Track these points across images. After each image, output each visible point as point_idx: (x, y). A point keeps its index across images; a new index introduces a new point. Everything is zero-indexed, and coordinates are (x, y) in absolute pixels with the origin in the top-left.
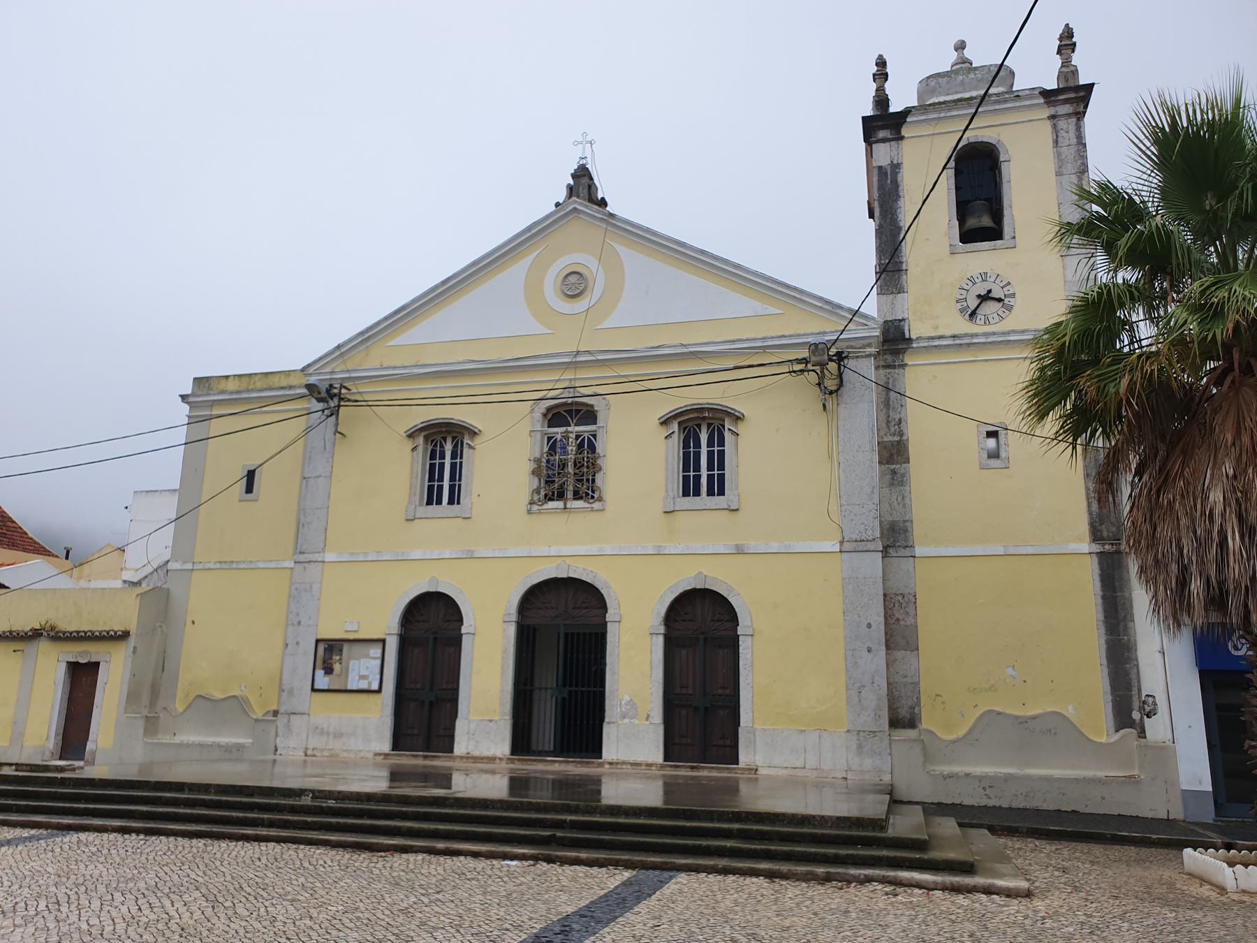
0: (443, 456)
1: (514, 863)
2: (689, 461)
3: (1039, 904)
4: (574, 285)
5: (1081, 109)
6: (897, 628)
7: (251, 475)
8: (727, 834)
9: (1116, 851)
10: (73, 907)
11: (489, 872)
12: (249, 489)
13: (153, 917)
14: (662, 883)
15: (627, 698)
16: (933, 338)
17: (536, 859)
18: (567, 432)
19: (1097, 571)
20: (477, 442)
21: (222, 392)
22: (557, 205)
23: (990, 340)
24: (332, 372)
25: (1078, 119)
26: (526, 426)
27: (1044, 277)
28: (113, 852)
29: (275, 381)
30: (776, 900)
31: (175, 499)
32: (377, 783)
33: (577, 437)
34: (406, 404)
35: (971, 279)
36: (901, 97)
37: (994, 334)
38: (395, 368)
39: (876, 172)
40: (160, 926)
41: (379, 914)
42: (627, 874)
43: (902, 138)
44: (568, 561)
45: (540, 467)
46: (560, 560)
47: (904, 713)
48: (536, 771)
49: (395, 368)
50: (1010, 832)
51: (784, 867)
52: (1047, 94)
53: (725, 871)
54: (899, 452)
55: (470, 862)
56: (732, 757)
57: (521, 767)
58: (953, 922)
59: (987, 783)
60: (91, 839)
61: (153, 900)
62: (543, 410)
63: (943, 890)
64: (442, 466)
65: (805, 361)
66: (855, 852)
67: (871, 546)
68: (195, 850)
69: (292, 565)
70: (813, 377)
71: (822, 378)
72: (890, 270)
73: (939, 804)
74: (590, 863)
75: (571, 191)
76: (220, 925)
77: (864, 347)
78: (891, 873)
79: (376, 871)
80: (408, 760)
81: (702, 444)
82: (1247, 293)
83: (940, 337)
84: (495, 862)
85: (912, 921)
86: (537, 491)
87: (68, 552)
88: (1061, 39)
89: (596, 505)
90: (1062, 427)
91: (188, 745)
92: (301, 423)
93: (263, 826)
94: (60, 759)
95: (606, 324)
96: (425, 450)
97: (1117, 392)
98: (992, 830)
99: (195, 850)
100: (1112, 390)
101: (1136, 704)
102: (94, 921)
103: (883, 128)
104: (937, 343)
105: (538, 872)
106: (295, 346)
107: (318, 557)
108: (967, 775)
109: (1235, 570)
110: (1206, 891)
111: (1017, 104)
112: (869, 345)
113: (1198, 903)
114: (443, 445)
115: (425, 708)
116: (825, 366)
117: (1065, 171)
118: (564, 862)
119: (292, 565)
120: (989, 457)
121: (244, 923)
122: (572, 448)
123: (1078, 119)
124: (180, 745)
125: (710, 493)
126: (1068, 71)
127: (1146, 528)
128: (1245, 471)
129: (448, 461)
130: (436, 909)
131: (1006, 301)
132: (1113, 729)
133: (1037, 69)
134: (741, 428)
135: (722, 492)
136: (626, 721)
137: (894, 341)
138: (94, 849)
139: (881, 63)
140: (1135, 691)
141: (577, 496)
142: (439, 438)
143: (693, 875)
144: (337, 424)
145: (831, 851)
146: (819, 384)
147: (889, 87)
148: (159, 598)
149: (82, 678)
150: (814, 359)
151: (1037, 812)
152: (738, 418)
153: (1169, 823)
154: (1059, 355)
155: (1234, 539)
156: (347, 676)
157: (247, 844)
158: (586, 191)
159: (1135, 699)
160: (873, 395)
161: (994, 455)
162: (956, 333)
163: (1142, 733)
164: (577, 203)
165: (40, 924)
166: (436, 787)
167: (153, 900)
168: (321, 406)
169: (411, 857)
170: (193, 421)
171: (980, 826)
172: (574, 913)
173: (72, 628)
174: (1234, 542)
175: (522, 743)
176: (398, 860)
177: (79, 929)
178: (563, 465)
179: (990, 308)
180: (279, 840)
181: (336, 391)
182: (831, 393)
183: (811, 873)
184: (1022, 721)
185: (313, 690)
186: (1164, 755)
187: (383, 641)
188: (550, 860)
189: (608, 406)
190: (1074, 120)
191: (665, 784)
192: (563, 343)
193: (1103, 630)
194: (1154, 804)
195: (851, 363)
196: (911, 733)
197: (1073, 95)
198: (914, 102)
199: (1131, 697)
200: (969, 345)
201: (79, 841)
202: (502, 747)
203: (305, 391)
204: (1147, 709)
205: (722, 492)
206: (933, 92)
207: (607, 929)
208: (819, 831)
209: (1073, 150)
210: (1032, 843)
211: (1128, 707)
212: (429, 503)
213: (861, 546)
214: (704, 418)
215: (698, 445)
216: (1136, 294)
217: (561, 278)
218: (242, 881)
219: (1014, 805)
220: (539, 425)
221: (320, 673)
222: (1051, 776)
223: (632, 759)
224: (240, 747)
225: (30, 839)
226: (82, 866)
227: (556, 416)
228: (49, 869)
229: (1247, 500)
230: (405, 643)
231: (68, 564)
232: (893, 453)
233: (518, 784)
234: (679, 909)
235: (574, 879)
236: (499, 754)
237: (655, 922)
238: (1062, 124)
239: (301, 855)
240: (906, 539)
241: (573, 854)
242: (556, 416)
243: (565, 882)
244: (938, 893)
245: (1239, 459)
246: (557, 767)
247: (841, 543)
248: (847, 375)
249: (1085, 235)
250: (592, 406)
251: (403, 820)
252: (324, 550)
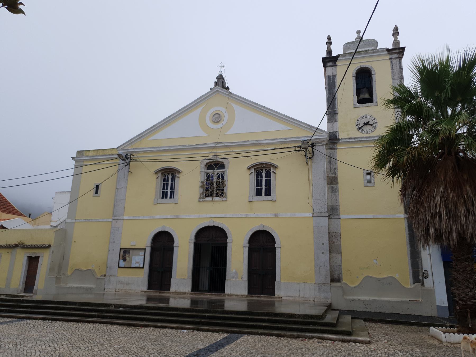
0: (168, 181)
1: (185, 331)
2: (258, 183)
3: (373, 346)
4: (217, 118)
5: (401, 56)
6: (333, 244)
7: (97, 187)
8: (264, 321)
9: (409, 328)
10: (22, 346)
11: (176, 334)
12: (97, 192)
13: (50, 350)
14: (238, 338)
15: (234, 271)
16: (347, 139)
17: (194, 329)
18: (214, 172)
19: (407, 224)
20: (180, 175)
21: (87, 156)
22: (211, 89)
23: (368, 139)
24: (128, 149)
25: (400, 60)
27: (385, 118)
28: (39, 327)
29: (107, 152)
30: (277, 345)
31: (68, 195)
32: (142, 302)
33: (217, 174)
34: (155, 161)
35: (361, 117)
36: (337, 50)
37: (369, 137)
39: (327, 78)
40: (52, 353)
41: (132, 349)
42: (226, 335)
43: (336, 65)
44: (213, 220)
45: (203, 184)
46: (210, 219)
47: (336, 276)
48: (201, 298)
50: (372, 321)
51: (282, 333)
52: (388, 50)
53: (261, 334)
54: (334, 180)
55: (170, 331)
56: (272, 292)
57: (195, 296)
58: (339, 352)
59: (366, 303)
60: (31, 322)
61: (51, 344)
62: (205, 164)
63: (339, 341)
64: (168, 184)
65: (300, 147)
66: (309, 327)
67: (324, 215)
68: (69, 326)
69: (112, 221)
70: (303, 153)
71: (306, 152)
72: (332, 112)
73: (348, 310)
74: (213, 331)
75: (216, 83)
76: (73, 353)
77: (322, 142)
78: (321, 335)
79: (134, 334)
80: (153, 293)
81: (263, 178)
82: (446, 127)
83: (350, 138)
84: (179, 331)
85: (324, 352)
86: (202, 194)
87: (30, 215)
88: (394, 30)
89: (224, 199)
90: (388, 173)
91: (72, 288)
92: (116, 168)
93: (95, 317)
94: (24, 293)
95: (228, 133)
96: (162, 178)
97: (403, 161)
98: (365, 320)
99: (69, 326)
100: (402, 160)
101: (421, 274)
102: (29, 351)
103: (329, 62)
104: (348, 140)
105: (194, 334)
106: (114, 140)
107: (121, 218)
108: (359, 300)
109: (444, 225)
110: (436, 343)
111: (378, 54)
112: (324, 141)
113: (431, 347)
114: (168, 177)
115: (160, 273)
116: (307, 148)
117: (395, 78)
118: (204, 330)
119: (112, 221)
120: (367, 182)
121: (82, 352)
122: (215, 178)
123: (400, 60)
124: (69, 288)
126: (396, 42)
127: (415, 210)
128: (448, 190)
129: (170, 182)
130: (153, 347)
131: (374, 125)
132: (412, 283)
133: (386, 42)
134: (277, 171)
135: (270, 195)
136: (234, 279)
137: (333, 139)
138: (32, 326)
139: (329, 38)
140: (420, 269)
141: (217, 195)
142: (166, 174)
143: (250, 336)
144: (129, 169)
145: (300, 327)
146: (305, 155)
147: (332, 47)
148: (63, 233)
149: (33, 262)
150: (303, 146)
151: (384, 314)
152: (276, 167)
153: (432, 318)
154: (384, 147)
155: (444, 214)
156: (131, 262)
157: (89, 324)
158: (222, 84)
159: (420, 272)
160: (326, 159)
161: (369, 181)
162: (356, 137)
163: (423, 285)
164: (219, 89)
165: (9, 352)
166: (160, 303)
167: (51, 344)
168: (123, 162)
169: (148, 329)
170: (76, 167)
171: (361, 319)
172: (202, 349)
173: (30, 243)
174: (444, 215)
175: (196, 287)
176: (143, 330)
177: (23, 354)
178: (212, 184)
179: (368, 127)
180: (100, 323)
181: (129, 156)
182: (309, 158)
183: (292, 335)
184: (379, 280)
185: (119, 267)
186: (431, 292)
187: (145, 249)
188: (198, 330)
189: (229, 162)
190: (398, 60)
191: (248, 303)
192: (212, 140)
193: (409, 246)
194: (427, 311)
195: (316, 148)
196: (338, 284)
197: (398, 51)
198: (342, 52)
199: (419, 271)
200: (360, 141)
201: (27, 323)
202: (188, 289)
203: (117, 156)
204: (425, 275)
205: (270, 195)
206: (348, 49)
207: (213, 354)
208: (297, 320)
209: (398, 70)
210: (379, 325)
211: (418, 274)
212: (163, 198)
213: (320, 215)
214: (264, 167)
215: (261, 177)
216: (410, 126)
217: (214, 114)
218: (84, 337)
219: (376, 311)
220: (204, 169)
221: (121, 261)
222: (388, 300)
223: (236, 293)
224: (91, 288)
225: (9, 322)
226: (27, 332)
227: (210, 166)
228: (15, 333)
229: (448, 200)
230: (153, 250)
231: (30, 219)
232: (333, 180)
233: (194, 302)
234: (241, 348)
235: (206, 337)
236: (187, 291)
237: (231, 352)
238: (394, 61)
239: (108, 328)
240: (337, 212)
241: (207, 328)
242: (210, 166)
243: (202, 338)
244: (337, 342)
245: (446, 185)
246: (208, 296)
247: (313, 213)
248: (315, 152)
249: (394, 104)
250: (223, 162)
251: (152, 315)
252: (123, 215)
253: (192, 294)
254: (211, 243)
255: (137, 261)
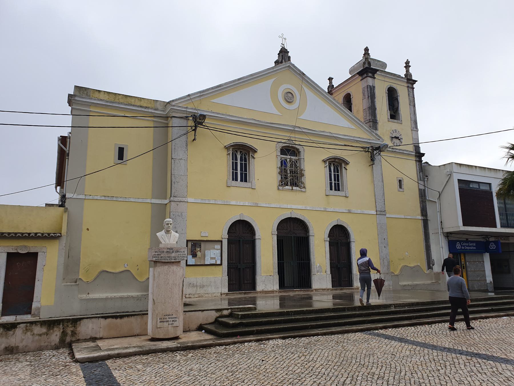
4: (289, 97)
12: (400, 187)
15: (318, 265)
26: (275, 154)
29: (133, 101)
34: (229, 132)
38: (218, 114)
49: (218, 114)
80: (237, 295)
115: (241, 271)
125: (335, 190)
147: (411, 70)
184: (412, 268)
185: (187, 265)
187: (221, 241)
236: (275, 289)
247: (376, 211)
253: (280, 292)
254: (293, 235)
255: (213, 256)
